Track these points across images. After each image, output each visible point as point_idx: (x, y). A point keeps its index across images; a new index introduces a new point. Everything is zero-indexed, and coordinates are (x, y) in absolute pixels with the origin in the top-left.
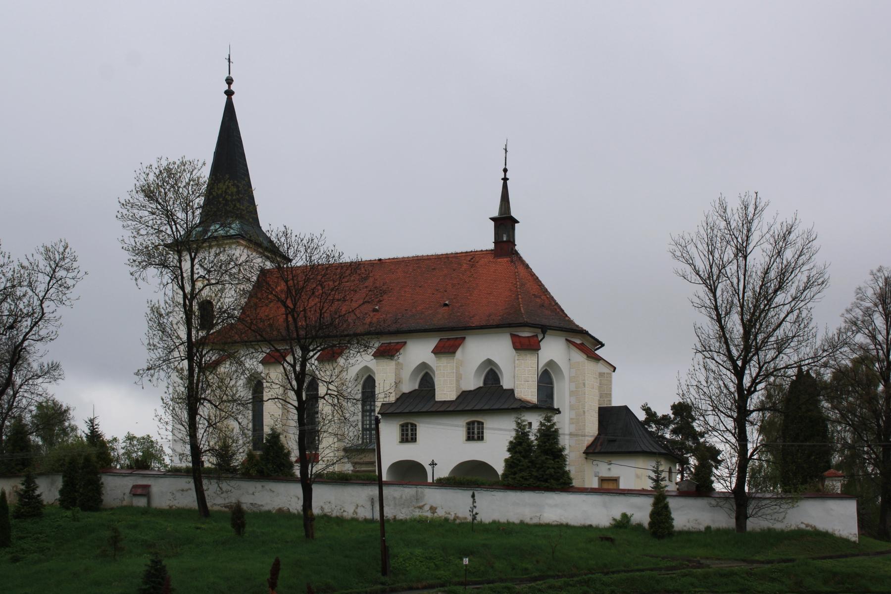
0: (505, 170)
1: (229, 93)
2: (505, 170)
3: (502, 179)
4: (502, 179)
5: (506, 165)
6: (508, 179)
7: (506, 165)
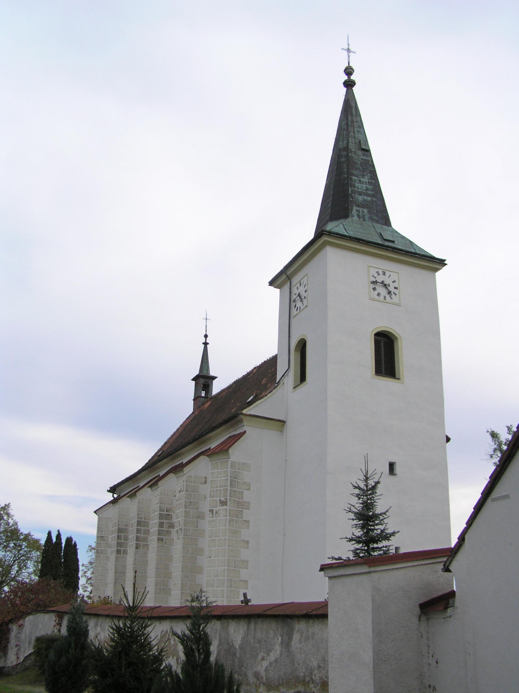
0: (206, 336)
1: (206, 344)
2: (206, 336)
3: (203, 343)
4: (203, 343)
5: (206, 331)
6: (208, 344)
7: (206, 331)
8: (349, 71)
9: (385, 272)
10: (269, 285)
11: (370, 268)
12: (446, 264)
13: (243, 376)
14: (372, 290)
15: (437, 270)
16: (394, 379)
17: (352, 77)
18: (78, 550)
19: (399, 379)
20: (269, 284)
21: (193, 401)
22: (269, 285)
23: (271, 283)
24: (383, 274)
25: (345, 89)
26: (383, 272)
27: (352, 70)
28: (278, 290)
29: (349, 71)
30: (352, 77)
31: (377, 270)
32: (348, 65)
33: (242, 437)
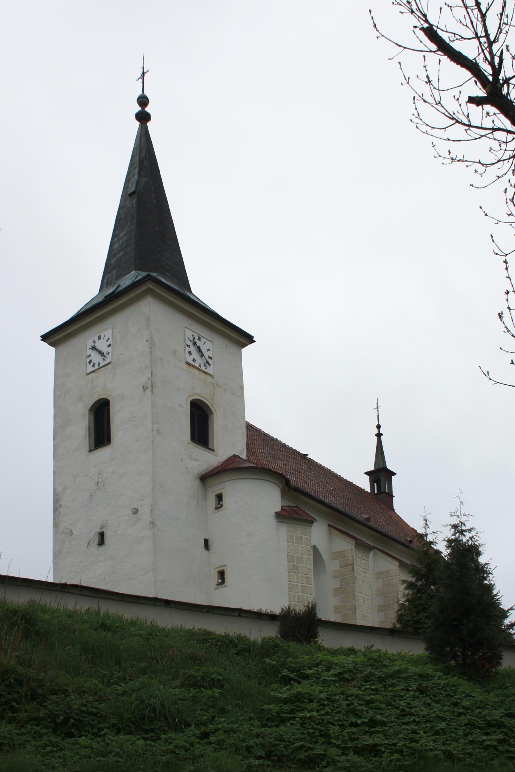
8: (143, 101)
9: (200, 338)
10: (41, 340)
11: (186, 329)
12: (254, 341)
13: (467, 57)
14: (187, 353)
15: (244, 345)
16: (206, 449)
17: (147, 109)
18: (450, 60)
19: (213, 450)
20: (41, 338)
21: (393, 495)
22: (41, 340)
23: (45, 338)
24: (198, 339)
25: (138, 123)
26: (198, 337)
27: (144, 99)
28: (53, 349)
29: (143, 101)
30: (147, 109)
31: (193, 333)
32: (141, 93)
33: (90, 586)
